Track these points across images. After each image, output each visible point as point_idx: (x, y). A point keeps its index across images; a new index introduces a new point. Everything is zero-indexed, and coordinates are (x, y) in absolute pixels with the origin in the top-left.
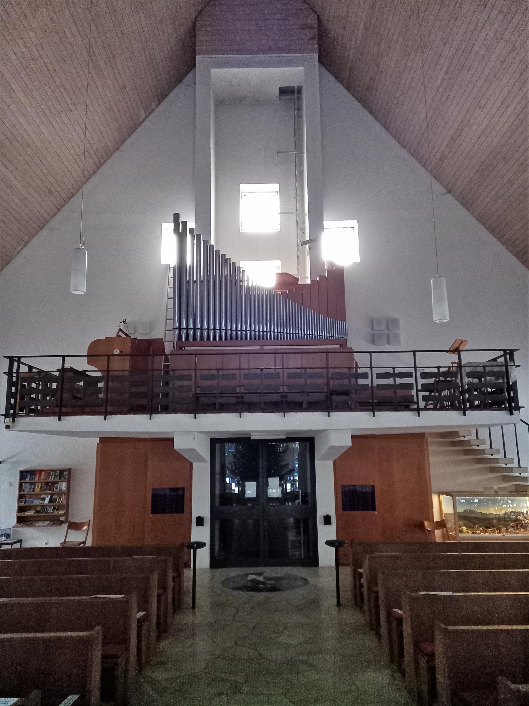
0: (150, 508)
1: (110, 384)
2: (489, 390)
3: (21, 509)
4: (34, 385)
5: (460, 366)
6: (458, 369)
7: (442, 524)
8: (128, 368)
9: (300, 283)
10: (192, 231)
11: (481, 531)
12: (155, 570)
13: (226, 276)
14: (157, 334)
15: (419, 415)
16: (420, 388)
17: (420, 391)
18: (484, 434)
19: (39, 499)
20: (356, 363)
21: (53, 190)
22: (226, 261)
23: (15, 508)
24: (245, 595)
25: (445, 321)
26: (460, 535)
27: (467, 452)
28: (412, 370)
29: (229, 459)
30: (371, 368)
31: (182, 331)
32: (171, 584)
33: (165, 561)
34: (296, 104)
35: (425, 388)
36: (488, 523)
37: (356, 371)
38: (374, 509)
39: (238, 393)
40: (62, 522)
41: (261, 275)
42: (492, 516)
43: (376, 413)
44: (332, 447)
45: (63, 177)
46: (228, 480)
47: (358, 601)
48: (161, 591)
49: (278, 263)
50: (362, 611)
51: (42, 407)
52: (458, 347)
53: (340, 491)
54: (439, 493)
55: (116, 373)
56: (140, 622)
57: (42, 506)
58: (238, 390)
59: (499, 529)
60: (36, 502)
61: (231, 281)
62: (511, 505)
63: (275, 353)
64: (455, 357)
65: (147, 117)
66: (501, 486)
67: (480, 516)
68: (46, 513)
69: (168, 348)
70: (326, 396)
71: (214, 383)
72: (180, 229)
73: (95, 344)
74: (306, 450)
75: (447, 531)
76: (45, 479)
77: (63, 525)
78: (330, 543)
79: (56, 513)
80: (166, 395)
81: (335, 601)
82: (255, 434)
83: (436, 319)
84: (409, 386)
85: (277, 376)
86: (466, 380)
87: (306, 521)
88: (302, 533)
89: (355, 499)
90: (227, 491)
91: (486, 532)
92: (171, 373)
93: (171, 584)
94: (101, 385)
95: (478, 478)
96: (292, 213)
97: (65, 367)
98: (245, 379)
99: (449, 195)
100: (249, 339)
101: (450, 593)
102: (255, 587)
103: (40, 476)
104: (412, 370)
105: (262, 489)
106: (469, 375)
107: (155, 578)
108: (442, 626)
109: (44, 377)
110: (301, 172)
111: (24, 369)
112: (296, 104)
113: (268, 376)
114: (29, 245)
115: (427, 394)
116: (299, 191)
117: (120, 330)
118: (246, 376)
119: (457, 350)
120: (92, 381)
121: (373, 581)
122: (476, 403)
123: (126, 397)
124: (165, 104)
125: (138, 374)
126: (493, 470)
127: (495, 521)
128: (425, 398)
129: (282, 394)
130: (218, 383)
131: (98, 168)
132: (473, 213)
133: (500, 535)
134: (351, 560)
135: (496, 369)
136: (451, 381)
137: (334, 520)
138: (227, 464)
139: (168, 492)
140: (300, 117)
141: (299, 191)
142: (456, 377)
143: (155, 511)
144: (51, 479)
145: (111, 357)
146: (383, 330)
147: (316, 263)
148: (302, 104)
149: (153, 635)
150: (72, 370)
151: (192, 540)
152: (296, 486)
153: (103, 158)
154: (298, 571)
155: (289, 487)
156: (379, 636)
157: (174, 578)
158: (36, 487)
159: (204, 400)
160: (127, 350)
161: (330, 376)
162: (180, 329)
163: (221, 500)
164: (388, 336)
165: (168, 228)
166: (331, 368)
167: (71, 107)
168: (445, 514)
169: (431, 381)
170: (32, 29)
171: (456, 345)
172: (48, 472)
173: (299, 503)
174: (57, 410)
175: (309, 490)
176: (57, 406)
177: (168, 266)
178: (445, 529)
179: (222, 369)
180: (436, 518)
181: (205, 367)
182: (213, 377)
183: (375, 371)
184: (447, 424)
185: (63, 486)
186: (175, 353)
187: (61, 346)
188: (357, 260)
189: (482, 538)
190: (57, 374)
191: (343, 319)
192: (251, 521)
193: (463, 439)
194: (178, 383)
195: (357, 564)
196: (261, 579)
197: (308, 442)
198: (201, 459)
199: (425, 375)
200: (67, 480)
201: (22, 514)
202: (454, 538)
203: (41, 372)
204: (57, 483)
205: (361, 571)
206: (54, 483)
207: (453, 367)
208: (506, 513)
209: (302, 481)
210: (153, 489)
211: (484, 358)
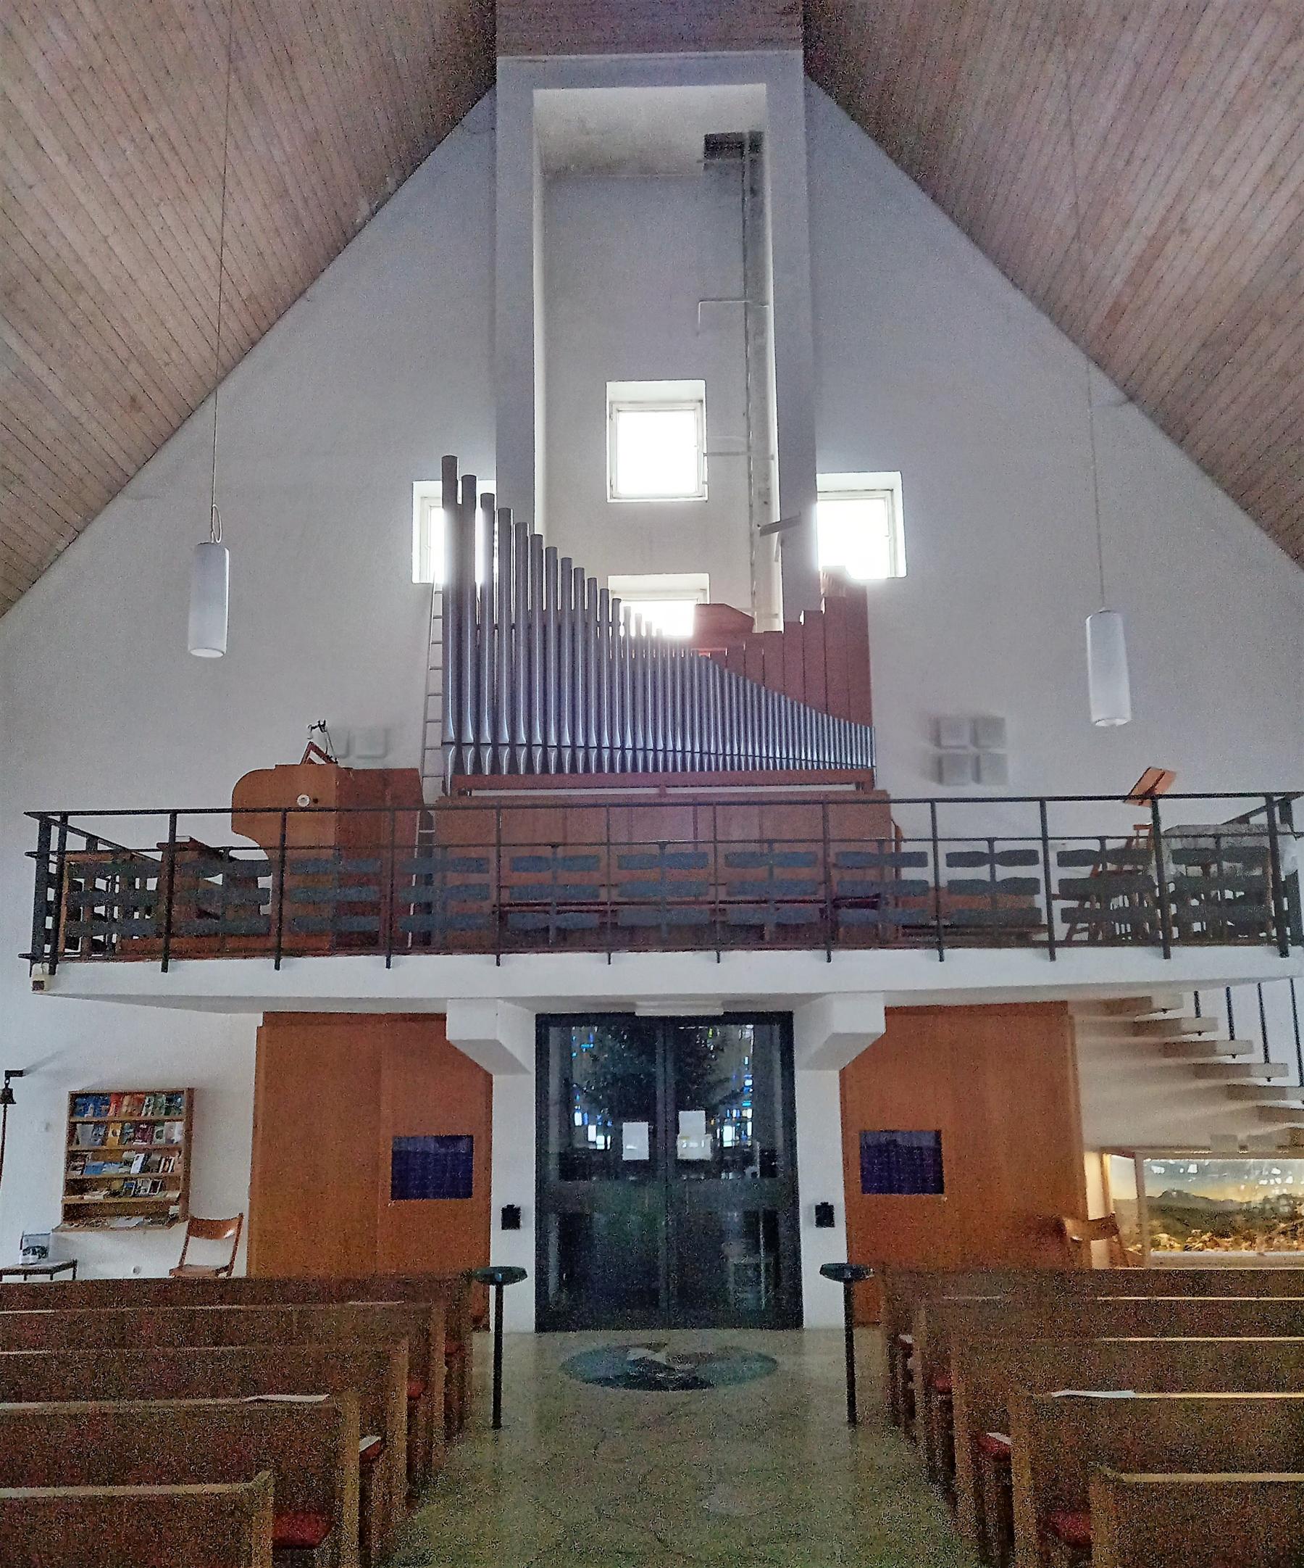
2: (1229, 894)
3: (74, 1187)
4: (101, 884)
7: (1107, 1226)
9: (757, 629)
10: (487, 499)
11: (1204, 1242)
14: (403, 757)
15: (1053, 958)
16: (1055, 890)
17: (1056, 897)
18: (1213, 1004)
20: (897, 827)
21: (142, 399)
22: (573, 574)
25: (1119, 722)
26: (1154, 1253)
27: (1169, 1049)
29: (582, 1069)
30: (935, 840)
32: (440, 1369)
35: (1068, 889)
36: (1223, 1223)
40: (174, 1219)
42: (1230, 1208)
47: (902, 1412)
49: (703, 579)
54: (1103, 1150)
56: (367, 1460)
58: (603, 895)
59: (1251, 1239)
60: (111, 1170)
61: (586, 625)
64: (1143, 814)
65: (373, 214)
66: (1255, 1132)
67: (1201, 1205)
69: (431, 791)
73: (254, 778)
75: (1120, 1242)
78: (831, 1271)
79: (158, 1196)
80: (427, 908)
82: (645, 1003)
83: (1099, 717)
84: (1029, 886)
86: (1171, 869)
87: (771, 1219)
89: (892, 1165)
90: (578, 1146)
91: (1217, 1245)
92: (438, 853)
93: (440, 1369)
95: (1195, 1115)
96: (738, 454)
98: (620, 867)
100: (630, 772)
101: (1129, 1394)
103: (118, 1106)
104: (1037, 846)
105: (663, 1137)
106: (1179, 857)
107: (402, 1359)
108: (1109, 1472)
110: (761, 350)
111: (76, 843)
114: (83, 539)
117: (312, 747)
119: (1149, 796)
120: (244, 875)
122: (1197, 927)
123: (328, 912)
126: (1236, 1093)
131: (253, 344)
132: (1190, 452)
133: (1252, 1253)
134: (882, 1316)
137: (840, 1215)
139: (432, 1147)
140: (758, 212)
144: (146, 1113)
148: (762, 175)
149: (401, 1488)
150: (194, 845)
151: (494, 1263)
155: (729, 1135)
156: (951, 1496)
158: (110, 1134)
160: (330, 799)
161: (832, 859)
162: (459, 744)
163: (565, 1166)
164: (977, 759)
165: (429, 490)
169: (1084, 872)
172: (138, 1097)
175: (780, 1144)
177: (428, 589)
180: (1095, 1212)
183: (944, 848)
187: (166, 784)
190: (158, 856)
194: (454, 879)
195: (900, 1323)
196: (660, 1357)
197: (777, 1023)
198: (512, 1065)
199: (1067, 859)
200: (183, 1116)
201: (75, 1199)
203: (119, 851)
204: (161, 1123)
205: (908, 1339)
206: (152, 1124)
207: (1138, 837)
208: (1266, 1200)
210: (398, 1140)
211: (1217, 814)
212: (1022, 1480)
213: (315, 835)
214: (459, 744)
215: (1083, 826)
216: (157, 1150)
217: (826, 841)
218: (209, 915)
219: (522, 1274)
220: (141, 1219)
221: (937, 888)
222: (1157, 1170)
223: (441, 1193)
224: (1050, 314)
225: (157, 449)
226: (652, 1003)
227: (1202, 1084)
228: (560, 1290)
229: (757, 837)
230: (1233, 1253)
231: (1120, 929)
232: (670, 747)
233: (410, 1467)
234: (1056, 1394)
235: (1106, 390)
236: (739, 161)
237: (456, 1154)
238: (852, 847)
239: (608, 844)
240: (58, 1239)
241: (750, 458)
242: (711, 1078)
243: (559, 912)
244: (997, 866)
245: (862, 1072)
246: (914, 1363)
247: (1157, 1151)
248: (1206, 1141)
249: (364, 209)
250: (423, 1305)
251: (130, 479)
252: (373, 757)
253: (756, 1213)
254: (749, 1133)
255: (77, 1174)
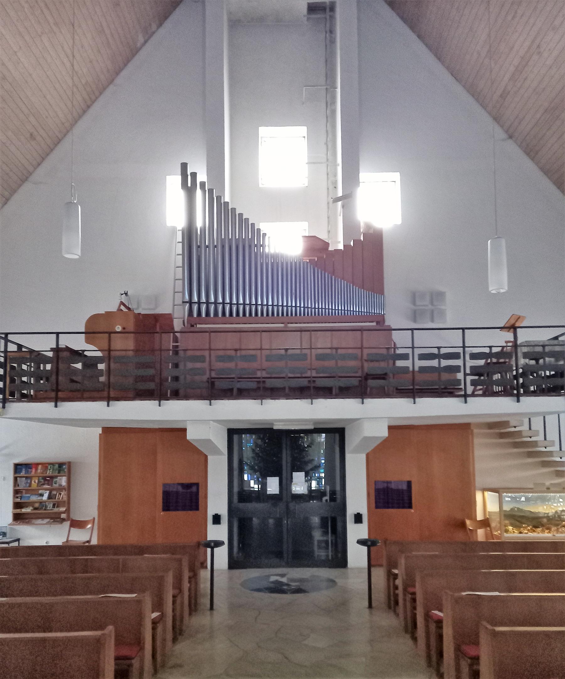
0: (161, 507)
1: (112, 365)
2: (548, 373)
3: (17, 505)
4: (24, 367)
5: (515, 345)
6: (514, 348)
7: (485, 523)
8: (132, 348)
9: (331, 248)
10: (203, 185)
11: (528, 530)
12: (170, 570)
13: (244, 240)
14: (165, 309)
15: (466, 402)
16: (468, 371)
17: (468, 375)
18: (537, 424)
19: (36, 495)
20: (394, 343)
21: (35, 133)
22: (243, 221)
24: (268, 597)
25: (502, 291)
26: (506, 535)
27: (516, 445)
28: (460, 350)
29: (248, 454)
30: (413, 348)
31: (193, 305)
32: (186, 585)
33: (180, 561)
34: (328, 25)
35: (475, 371)
36: (537, 522)
37: (394, 352)
38: (410, 507)
39: (259, 378)
40: (63, 520)
41: (284, 240)
42: (541, 515)
43: (417, 400)
44: (367, 439)
45: (47, 117)
46: (246, 477)
47: (392, 603)
48: (191, 574)
49: (305, 225)
50: (397, 615)
51: (35, 391)
52: (514, 324)
53: (373, 487)
54: (484, 490)
55: (118, 353)
56: (155, 623)
57: (41, 503)
58: (259, 374)
59: (549, 529)
60: (34, 498)
61: (250, 246)
62: (562, 504)
63: (301, 331)
64: (509, 336)
65: (146, 42)
66: (553, 482)
67: (527, 514)
68: (45, 510)
69: (178, 325)
70: (360, 381)
71: (232, 365)
72: (189, 184)
73: (94, 319)
74: (335, 442)
75: (491, 530)
76: (42, 473)
77: (65, 523)
78: (361, 542)
79: (56, 510)
80: (176, 379)
81: (366, 603)
82: (278, 423)
83: (493, 289)
84: (457, 369)
85: (303, 357)
86: (522, 361)
87: (334, 520)
88: (330, 531)
89: (389, 497)
90: (246, 489)
91: (534, 531)
92: (181, 353)
93: (186, 585)
94: (101, 366)
95: (530, 474)
96: (321, 163)
97: (60, 346)
98: (266, 361)
99: (510, 141)
100: (271, 316)
101: (497, 593)
102: (277, 589)
103: (36, 469)
104: (460, 350)
105: (285, 485)
106: (525, 355)
107: (170, 579)
108: (489, 627)
109: (36, 357)
110: (334, 112)
111: (12, 348)
112: (328, 25)
113: (295, 358)
114: (10, 203)
115: (477, 377)
116: (330, 136)
117: (122, 303)
118: (268, 358)
119: (513, 328)
120: (90, 363)
121: (409, 583)
122: (532, 388)
123: (131, 380)
124: (168, 24)
125: (141, 355)
126: (545, 464)
127: (545, 520)
128: (473, 383)
129: (309, 379)
130: (236, 365)
131: (89, 107)
132: (537, 164)
133: (550, 535)
134: (384, 562)
135: (557, 349)
136: (505, 363)
137: (365, 519)
138: (245, 459)
139: (180, 489)
140: (333, 41)
141: (330, 136)
142: (510, 358)
143: (167, 506)
144: (49, 473)
145: (112, 335)
146: (425, 305)
147: (350, 226)
148: (335, 24)
149: (169, 636)
150: (68, 349)
151: (208, 539)
152: (322, 484)
153: (95, 93)
154: (324, 573)
155: (314, 484)
156: (414, 639)
157: (190, 578)
158: (33, 482)
159: (219, 384)
160: (131, 327)
161: (365, 357)
162: (191, 303)
163: (240, 497)
164: (432, 312)
165: (174, 182)
166: (366, 348)
167: (54, 28)
168: (489, 512)
169: (481, 362)
171: (512, 322)
172: (45, 465)
173: (326, 500)
174: (53, 395)
175: (338, 488)
176: (53, 390)
177: (174, 230)
178: (488, 529)
179: (240, 350)
180: (480, 516)
181: (221, 347)
182: (230, 359)
183: (417, 352)
184: (498, 412)
185: (63, 481)
186: (187, 330)
187: (53, 321)
188: (399, 221)
189: (529, 538)
190: (50, 354)
191: (380, 290)
192: (271, 521)
193: (513, 429)
194: (190, 365)
195: (392, 564)
196: (284, 580)
197: (337, 433)
198: (216, 451)
199: (474, 356)
200: (67, 474)
201: (18, 511)
202: (498, 537)
203: (31, 351)
204: (56, 477)
205: (396, 571)
206: (52, 477)
207: (507, 346)
208: (556, 512)
209: (330, 477)
210: (165, 485)
211: (544, 336)
212: (448, 632)
213: (124, 344)
214: (191, 303)
215: (480, 341)
216: (54, 489)
217: (362, 348)
218: (76, 382)
219: (222, 543)
220: (48, 520)
221: (413, 371)
222: (507, 499)
223: (184, 508)
224: (473, 96)
225: (43, 159)
226: (281, 423)
227: (530, 460)
228: (238, 553)
229: (329, 346)
230: (541, 535)
231: (496, 388)
232: (290, 304)
233: (174, 627)
234: (464, 594)
235: (500, 133)
236: (323, 16)
237: (192, 492)
238: (374, 351)
239: (261, 349)
240: (11, 529)
241: (328, 165)
242: (306, 459)
243: (239, 381)
244: (437, 366)
245: (377, 455)
246: (399, 582)
247: (509, 490)
248: (531, 486)
249: (141, 39)
250: (178, 556)
251: (30, 174)
252: (149, 309)
253: (327, 518)
254: (323, 484)
255: (18, 500)
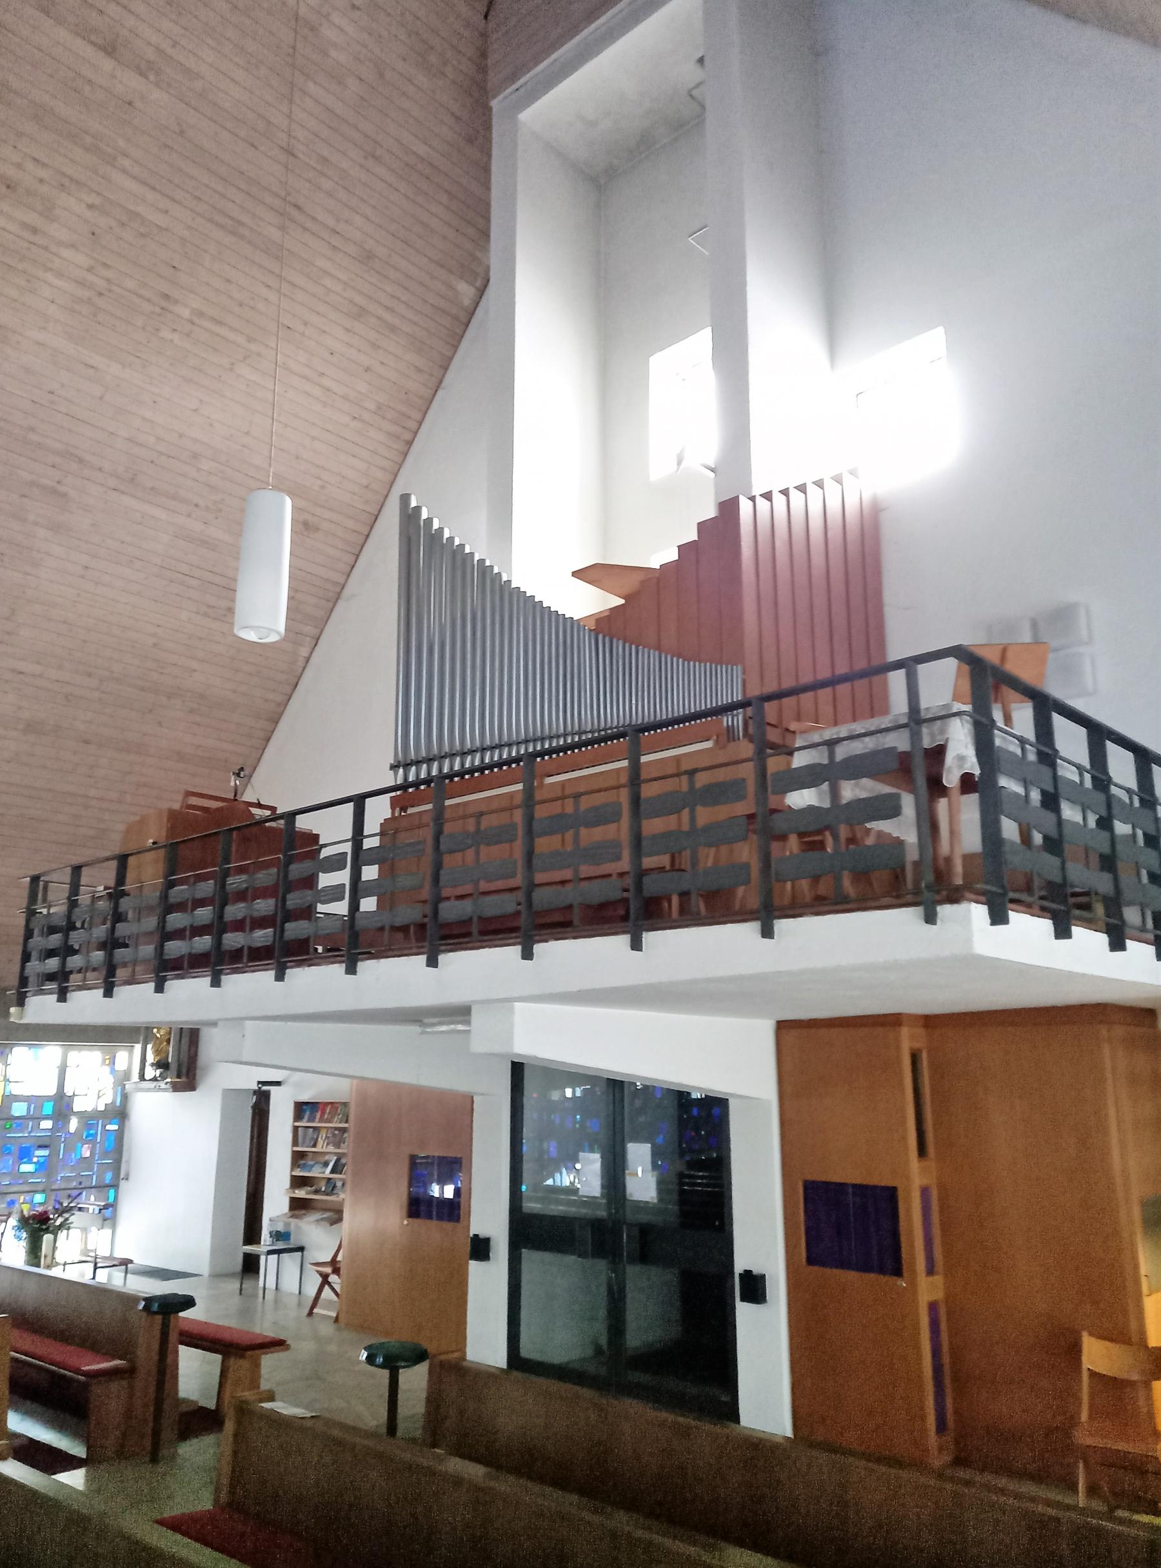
23: (287, 1183)
65: (482, 291)
89: (844, 1225)
131: (410, 443)
170: (61, 243)
